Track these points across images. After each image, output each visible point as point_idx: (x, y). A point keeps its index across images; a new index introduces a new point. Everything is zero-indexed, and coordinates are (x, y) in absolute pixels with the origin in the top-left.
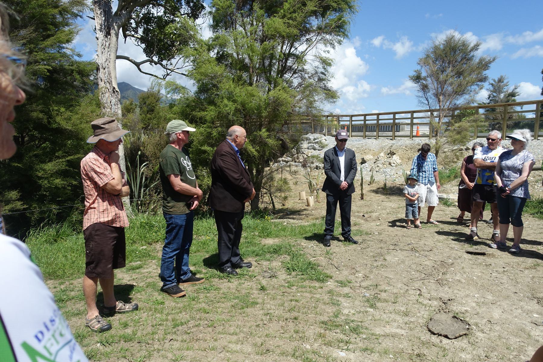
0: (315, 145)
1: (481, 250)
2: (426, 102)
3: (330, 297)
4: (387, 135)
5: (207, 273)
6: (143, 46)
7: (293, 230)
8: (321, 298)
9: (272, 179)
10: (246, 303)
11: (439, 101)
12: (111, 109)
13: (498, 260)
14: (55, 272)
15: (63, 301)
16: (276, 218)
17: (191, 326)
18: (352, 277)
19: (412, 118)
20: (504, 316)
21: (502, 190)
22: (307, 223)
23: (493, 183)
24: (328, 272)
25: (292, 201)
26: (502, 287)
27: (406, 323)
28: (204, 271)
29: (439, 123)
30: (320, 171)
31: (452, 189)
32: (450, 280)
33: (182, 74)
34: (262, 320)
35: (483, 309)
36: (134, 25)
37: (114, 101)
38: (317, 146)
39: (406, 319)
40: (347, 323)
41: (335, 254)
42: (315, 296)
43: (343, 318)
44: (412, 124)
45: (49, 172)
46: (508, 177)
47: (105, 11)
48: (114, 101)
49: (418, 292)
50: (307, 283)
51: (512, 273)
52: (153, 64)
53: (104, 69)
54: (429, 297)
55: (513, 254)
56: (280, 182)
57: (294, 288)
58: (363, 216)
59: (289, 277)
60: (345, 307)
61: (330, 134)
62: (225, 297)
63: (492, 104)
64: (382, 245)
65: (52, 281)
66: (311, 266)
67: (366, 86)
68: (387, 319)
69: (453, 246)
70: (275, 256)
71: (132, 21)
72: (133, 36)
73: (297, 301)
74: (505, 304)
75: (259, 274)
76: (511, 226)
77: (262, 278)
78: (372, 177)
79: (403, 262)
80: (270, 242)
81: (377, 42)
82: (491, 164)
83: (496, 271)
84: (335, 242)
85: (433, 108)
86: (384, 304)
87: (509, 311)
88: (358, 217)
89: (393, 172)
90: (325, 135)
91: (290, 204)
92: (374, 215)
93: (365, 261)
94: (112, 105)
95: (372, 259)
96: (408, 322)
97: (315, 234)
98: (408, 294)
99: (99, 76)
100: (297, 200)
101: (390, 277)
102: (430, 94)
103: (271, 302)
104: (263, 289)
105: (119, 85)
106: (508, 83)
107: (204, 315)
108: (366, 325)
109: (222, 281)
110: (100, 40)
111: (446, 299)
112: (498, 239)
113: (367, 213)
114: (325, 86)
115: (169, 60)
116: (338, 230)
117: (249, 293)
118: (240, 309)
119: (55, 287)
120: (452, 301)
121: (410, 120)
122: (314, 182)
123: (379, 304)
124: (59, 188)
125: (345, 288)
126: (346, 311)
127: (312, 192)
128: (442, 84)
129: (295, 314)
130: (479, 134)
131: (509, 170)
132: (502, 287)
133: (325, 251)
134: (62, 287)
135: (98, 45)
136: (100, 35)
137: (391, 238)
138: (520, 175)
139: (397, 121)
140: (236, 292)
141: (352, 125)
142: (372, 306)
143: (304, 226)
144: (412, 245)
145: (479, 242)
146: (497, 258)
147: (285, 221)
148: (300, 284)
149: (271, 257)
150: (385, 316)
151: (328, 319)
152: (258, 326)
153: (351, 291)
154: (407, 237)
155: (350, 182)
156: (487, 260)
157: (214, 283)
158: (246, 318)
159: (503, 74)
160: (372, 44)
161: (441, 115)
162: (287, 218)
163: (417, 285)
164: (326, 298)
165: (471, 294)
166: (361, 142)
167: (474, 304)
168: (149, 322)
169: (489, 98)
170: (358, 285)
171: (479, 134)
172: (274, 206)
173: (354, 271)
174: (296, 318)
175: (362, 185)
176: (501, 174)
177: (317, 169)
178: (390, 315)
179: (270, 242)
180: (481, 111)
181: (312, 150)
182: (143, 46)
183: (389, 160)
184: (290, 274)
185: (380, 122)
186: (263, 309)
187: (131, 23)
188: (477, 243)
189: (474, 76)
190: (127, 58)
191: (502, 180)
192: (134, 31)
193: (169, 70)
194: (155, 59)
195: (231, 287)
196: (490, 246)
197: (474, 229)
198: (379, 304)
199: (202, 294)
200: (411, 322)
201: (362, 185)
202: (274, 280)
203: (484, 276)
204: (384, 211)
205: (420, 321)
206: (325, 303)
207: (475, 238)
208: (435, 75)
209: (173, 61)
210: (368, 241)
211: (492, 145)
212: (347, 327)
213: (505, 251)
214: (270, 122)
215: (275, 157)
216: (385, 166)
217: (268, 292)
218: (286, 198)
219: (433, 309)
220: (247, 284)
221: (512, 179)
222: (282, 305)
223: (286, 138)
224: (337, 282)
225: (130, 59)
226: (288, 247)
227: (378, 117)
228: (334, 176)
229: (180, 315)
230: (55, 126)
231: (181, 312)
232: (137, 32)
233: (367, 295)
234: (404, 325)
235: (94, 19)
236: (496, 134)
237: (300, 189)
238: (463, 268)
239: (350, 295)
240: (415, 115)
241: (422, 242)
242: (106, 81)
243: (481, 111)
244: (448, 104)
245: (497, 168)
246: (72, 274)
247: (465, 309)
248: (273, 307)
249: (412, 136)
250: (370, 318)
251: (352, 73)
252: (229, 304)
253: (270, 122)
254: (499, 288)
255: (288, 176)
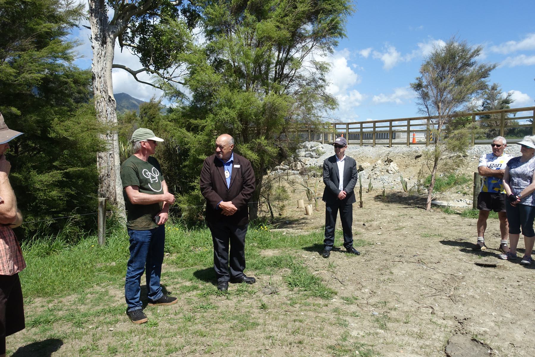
0: (312, 153)
1: (491, 262)
2: (426, 109)
3: (337, 316)
4: (383, 142)
5: (204, 289)
6: (140, 55)
7: (293, 240)
8: (327, 318)
9: (270, 187)
10: (245, 324)
11: (438, 108)
12: (107, 118)
13: (510, 273)
14: (43, 289)
15: (50, 322)
16: (275, 228)
17: (186, 352)
18: (357, 293)
19: (409, 125)
20: (527, 338)
21: (512, 198)
22: (307, 233)
23: (499, 191)
24: (333, 287)
25: (290, 209)
26: (520, 304)
27: (421, 347)
28: (201, 287)
29: (438, 129)
30: (317, 178)
31: (451, 196)
32: (463, 296)
33: (179, 83)
34: (264, 344)
35: (503, 330)
36: (130, 35)
37: (109, 110)
38: (314, 154)
39: (421, 342)
40: (358, 348)
41: (338, 267)
42: (320, 315)
43: (352, 341)
44: (409, 132)
45: (46, 183)
46: (518, 184)
47: (101, 20)
48: (109, 110)
49: (431, 310)
50: (310, 300)
51: (528, 288)
52: (150, 72)
53: (100, 78)
54: (442, 316)
55: (526, 266)
56: (278, 190)
57: (298, 306)
58: (364, 224)
59: (291, 293)
60: (354, 329)
61: (327, 142)
62: (224, 317)
63: (486, 111)
64: (387, 257)
65: (40, 299)
66: (314, 281)
67: (358, 96)
68: (400, 343)
69: (461, 257)
70: (275, 269)
71: (129, 30)
72: (130, 45)
73: (301, 321)
74: (526, 323)
75: (259, 290)
76: (521, 236)
77: (262, 294)
78: (370, 184)
79: (411, 276)
80: (269, 253)
81: (365, 53)
82: (497, 172)
83: (511, 285)
84: (338, 253)
85: (432, 115)
86: (395, 325)
87: (532, 332)
88: (359, 226)
89: (391, 179)
90: (321, 143)
91: (287, 213)
92: (375, 223)
93: (371, 275)
94: (107, 114)
95: (378, 273)
96: (423, 346)
97: (315, 244)
98: (420, 312)
99: (94, 85)
100: (295, 209)
101: (399, 292)
102: (430, 102)
103: (273, 323)
104: (264, 307)
105: (115, 96)
106: (500, 90)
107: (201, 339)
108: (378, 349)
109: (219, 298)
110: (96, 49)
111: (462, 318)
112: (508, 250)
113: (367, 221)
114: (324, 93)
115: (165, 69)
116: (339, 240)
117: (249, 312)
118: (240, 331)
119: (43, 306)
120: (469, 321)
121: (406, 127)
122: (312, 190)
123: (390, 325)
124: (54, 200)
125: (352, 306)
126: (354, 333)
127: (310, 200)
128: (441, 91)
129: (300, 337)
130: (477, 141)
131: (519, 177)
132: (520, 304)
133: (328, 263)
134: (51, 305)
135: (94, 54)
136: (96, 44)
137: (395, 248)
138: (531, 182)
139: (393, 128)
140: (235, 311)
141: (348, 133)
142: (382, 327)
143: (304, 236)
144: (418, 257)
145: (486, 252)
146: (509, 270)
147: (284, 231)
148: (303, 302)
149: (271, 270)
150: (397, 338)
151: (336, 342)
152: (259, 352)
153: (358, 308)
154: (412, 247)
155: (348, 192)
156: (499, 272)
157: (211, 301)
158: (246, 343)
159: (496, 82)
160: (361, 55)
161: (440, 121)
162: (286, 228)
163: (429, 301)
164: (332, 317)
165: (488, 312)
166: (358, 150)
167: (493, 324)
168: (140, 347)
169: (483, 106)
170: (365, 302)
171: (477, 141)
172: (272, 215)
173: (359, 286)
174: (300, 342)
175: (360, 193)
176: (510, 181)
177: (314, 177)
178: (403, 337)
179: (269, 253)
180: (477, 118)
181: (309, 158)
182: (140, 55)
183: (386, 167)
184: (292, 290)
185: (377, 129)
186: (264, 331)
187: (128, 33)
188: (485, 254)
189: (475, 83)
190: (123, 67)
191: (511, 188)
192: (130, 40)
193: (166, 78)
194: (152, 68)
195: (230, 305)
196: (500, 258)
197: (481, 238)
198: (390, 325)
199: (199, 314)
200: (427, 346)
201: (360, 193)
202: (275, 296)
203: (499, 292)
204: (385, 220)
205: (437, 344)
206: (331, 324)
207: (483, 248)
208: (435, 82)
209: (170, 70)
210: (372, 252)
211: (497, 152)
212: (357, 352)
213: (516, 263)
214: (268, 130)
215: (272, 166)
216: (383, 173)
217: (269, 310)
218: (282, 208)
219: (449, 330)
220: (247, 302)
221: (522, 187)
222: (285, 326)
223: (285, 146)
224: (343, 298)
225: (127, 67)
226: (289, 260)
227: (374, 125)
228: (332, 185)
229: (174, 338)
230: (53, 135)
231: (175, 335)
232: (133, 42)
233: (376, 313)
234: (419, 349)
235: (90, 28)
236: (501, 140)
237: (298, 197)
238: (475, 282)
239: (357, 314)
240: (412, 122)
241: (428, 254)
242: (102, 90)
243: (477, 118)
244: (447, 111)
245: (505, 176)
246: (62, 291)
247: (484, 329)
248: (275, 329)
249: (408, 144)
250: (381, 341)
251: (350, 80)
252: (228, 325)
253: (268, 130)
254: (517, 305)
255: (287, 185)
